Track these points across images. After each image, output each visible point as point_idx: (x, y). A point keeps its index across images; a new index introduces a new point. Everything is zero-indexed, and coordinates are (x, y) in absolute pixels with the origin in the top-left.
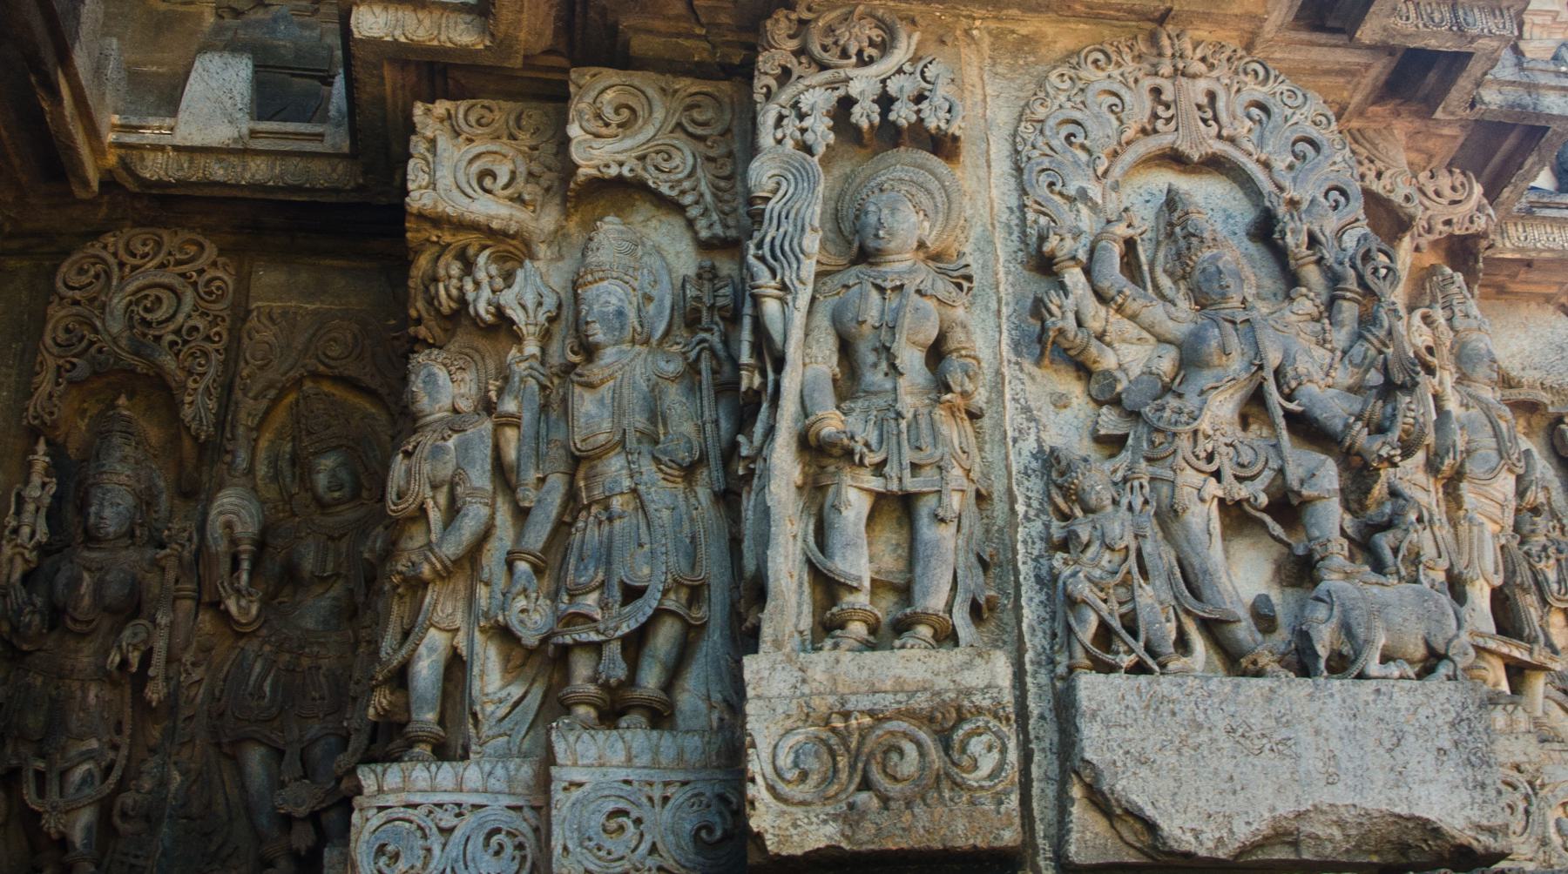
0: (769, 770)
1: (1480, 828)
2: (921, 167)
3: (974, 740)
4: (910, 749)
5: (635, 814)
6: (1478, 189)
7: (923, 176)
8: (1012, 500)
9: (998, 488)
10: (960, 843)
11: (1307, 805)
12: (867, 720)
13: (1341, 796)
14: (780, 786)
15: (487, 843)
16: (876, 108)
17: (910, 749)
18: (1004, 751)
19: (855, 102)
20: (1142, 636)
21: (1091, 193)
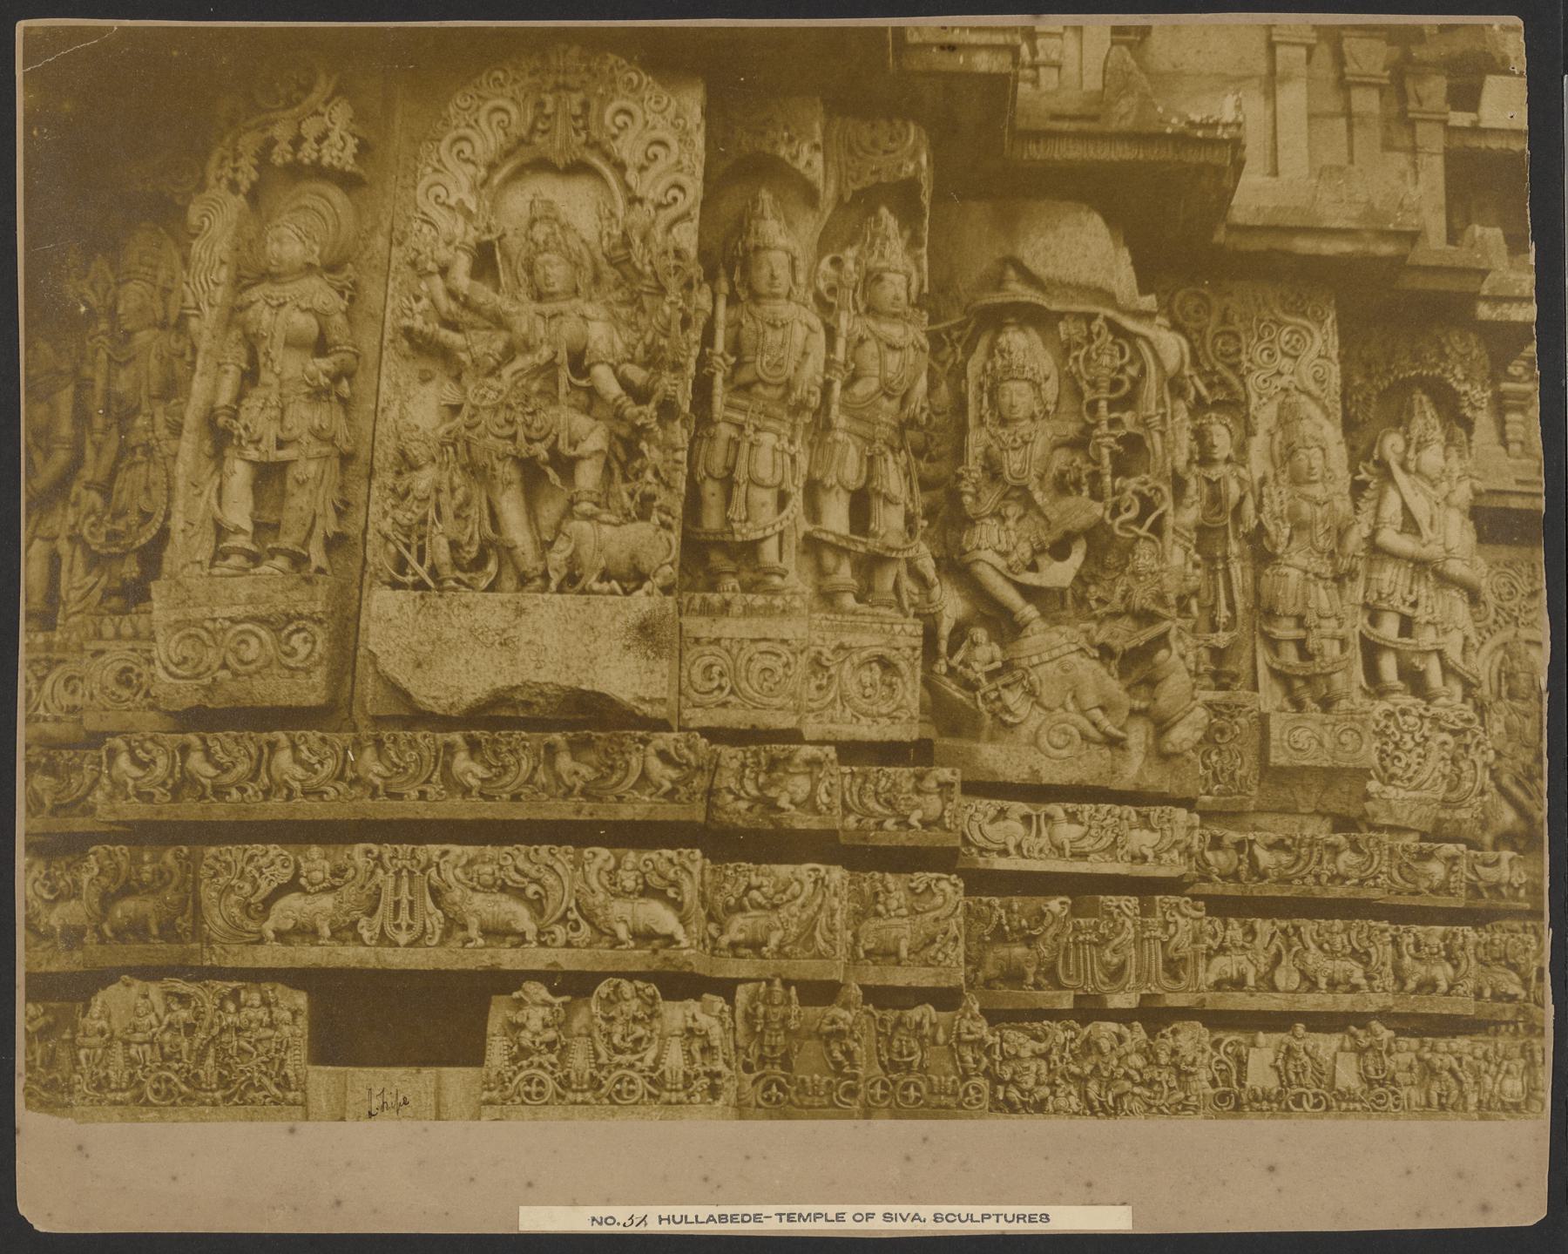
0: (163, 658)
1: (643, 700)
2: (322, 196)
3: (295, 637)
4: (254, 642)
5: (137, 670)
6: (1377, 205)
7: (320, 204)
8: (456, 452)
9: (364, 453)
10: (281, 703)
11: (517, 681)
12: (227, 623)
13: (544, 676)
14: (173, 668)
15: (66, 686)
16: (290, 148)
17: (254, 642)
18: (314, 643)
19: (276, 143)
20: (428, 563)
21: (468, 204)
